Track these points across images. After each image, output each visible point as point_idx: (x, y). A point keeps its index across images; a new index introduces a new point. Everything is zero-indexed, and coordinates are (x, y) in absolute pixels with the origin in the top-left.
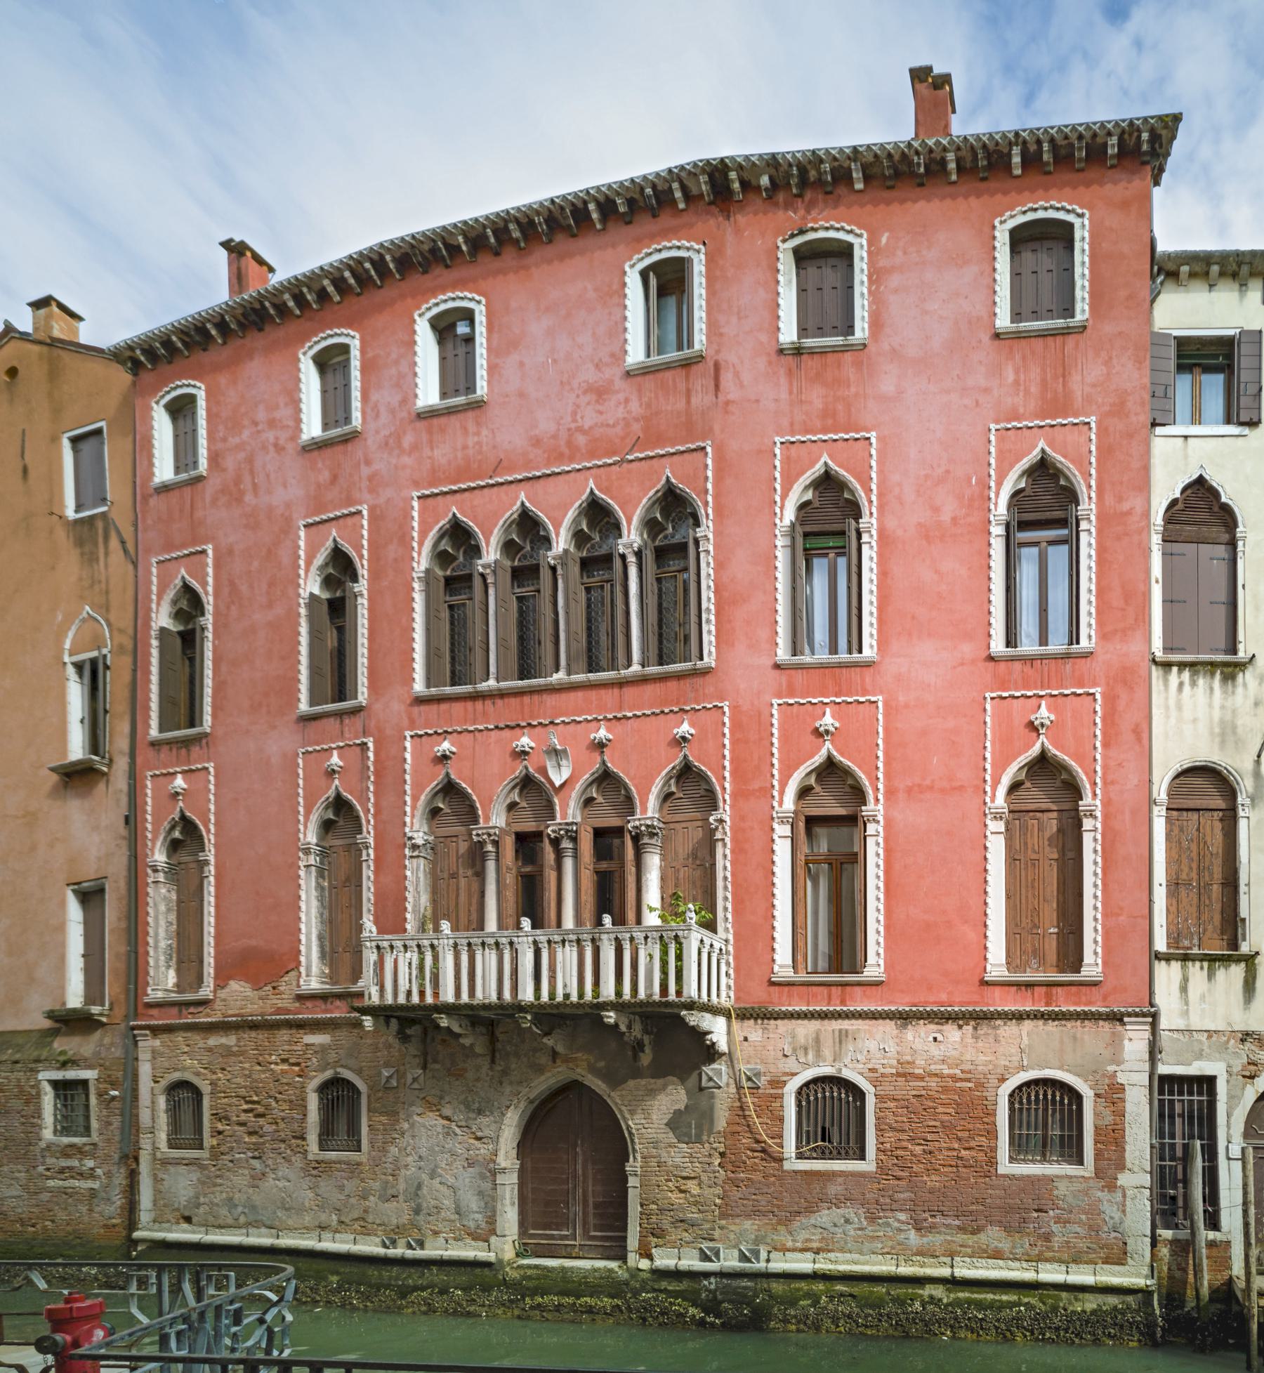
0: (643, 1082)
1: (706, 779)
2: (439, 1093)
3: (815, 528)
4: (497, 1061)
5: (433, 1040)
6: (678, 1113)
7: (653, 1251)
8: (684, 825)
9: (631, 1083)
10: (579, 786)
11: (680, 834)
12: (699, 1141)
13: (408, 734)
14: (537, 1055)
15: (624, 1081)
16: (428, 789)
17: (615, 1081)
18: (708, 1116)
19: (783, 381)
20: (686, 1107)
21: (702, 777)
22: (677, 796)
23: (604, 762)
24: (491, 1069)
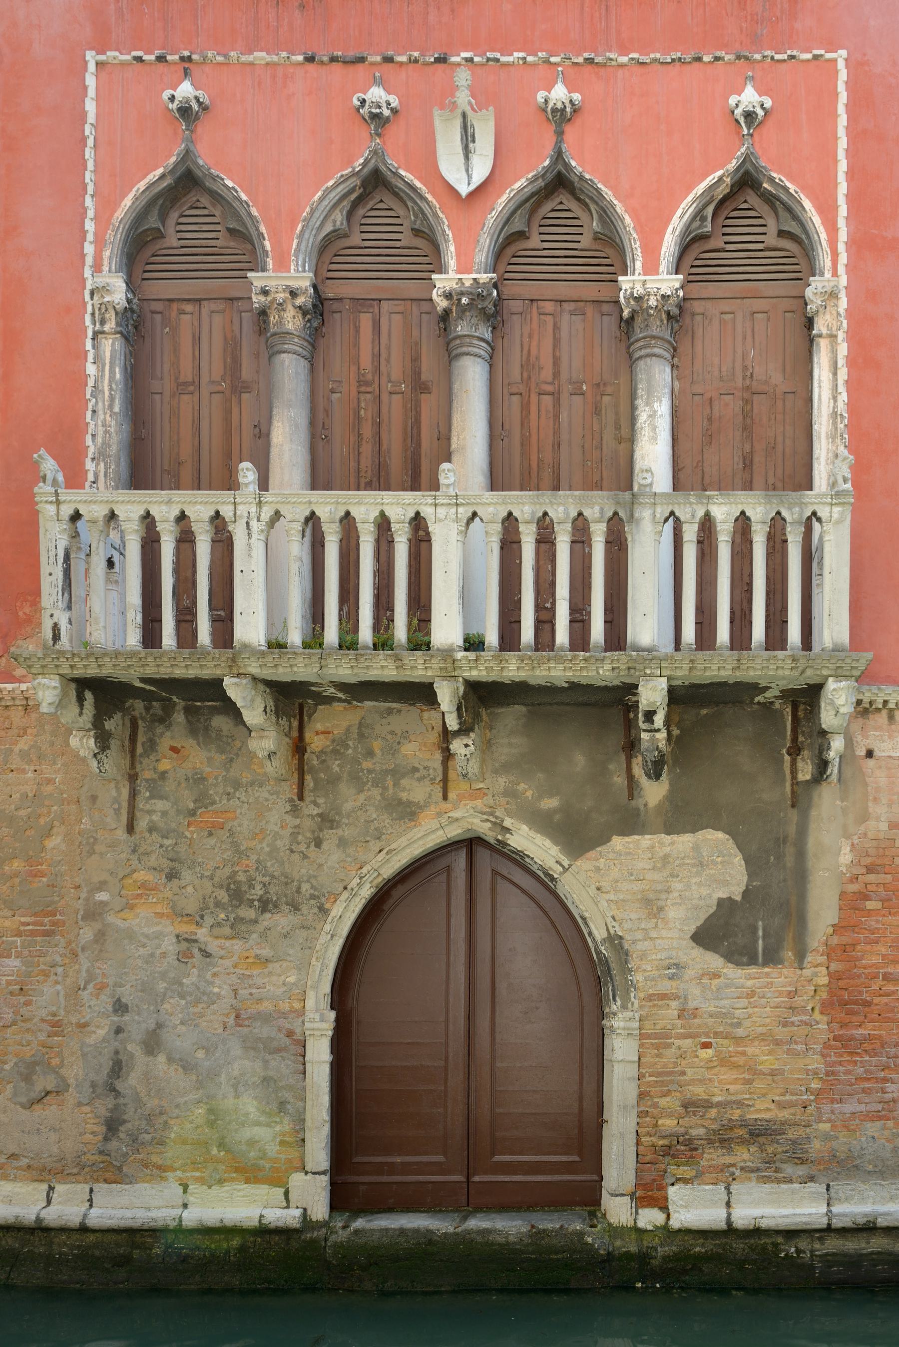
0: (646, 840)
1: (792, 212)
2: (165, 864)
3: (352, 480)
4: (309, 796)
5: (152, 745)
6: (726, 906)
7: (672, 1191)
8: (725, 306)
9: (618, 842)
10: (502, 202)
11: (716, 322)
12: (772, 958)
13: (91, 57)
14: (404, 782)
15: (604, 839)
16: (142, 185)
17: (578, 836)
18: (794, 914)
19: (289, 641)
20: (746, 894)
21: (779, 204)
22: (713, 244)
23: (559, 155)
24: (295, 811)
